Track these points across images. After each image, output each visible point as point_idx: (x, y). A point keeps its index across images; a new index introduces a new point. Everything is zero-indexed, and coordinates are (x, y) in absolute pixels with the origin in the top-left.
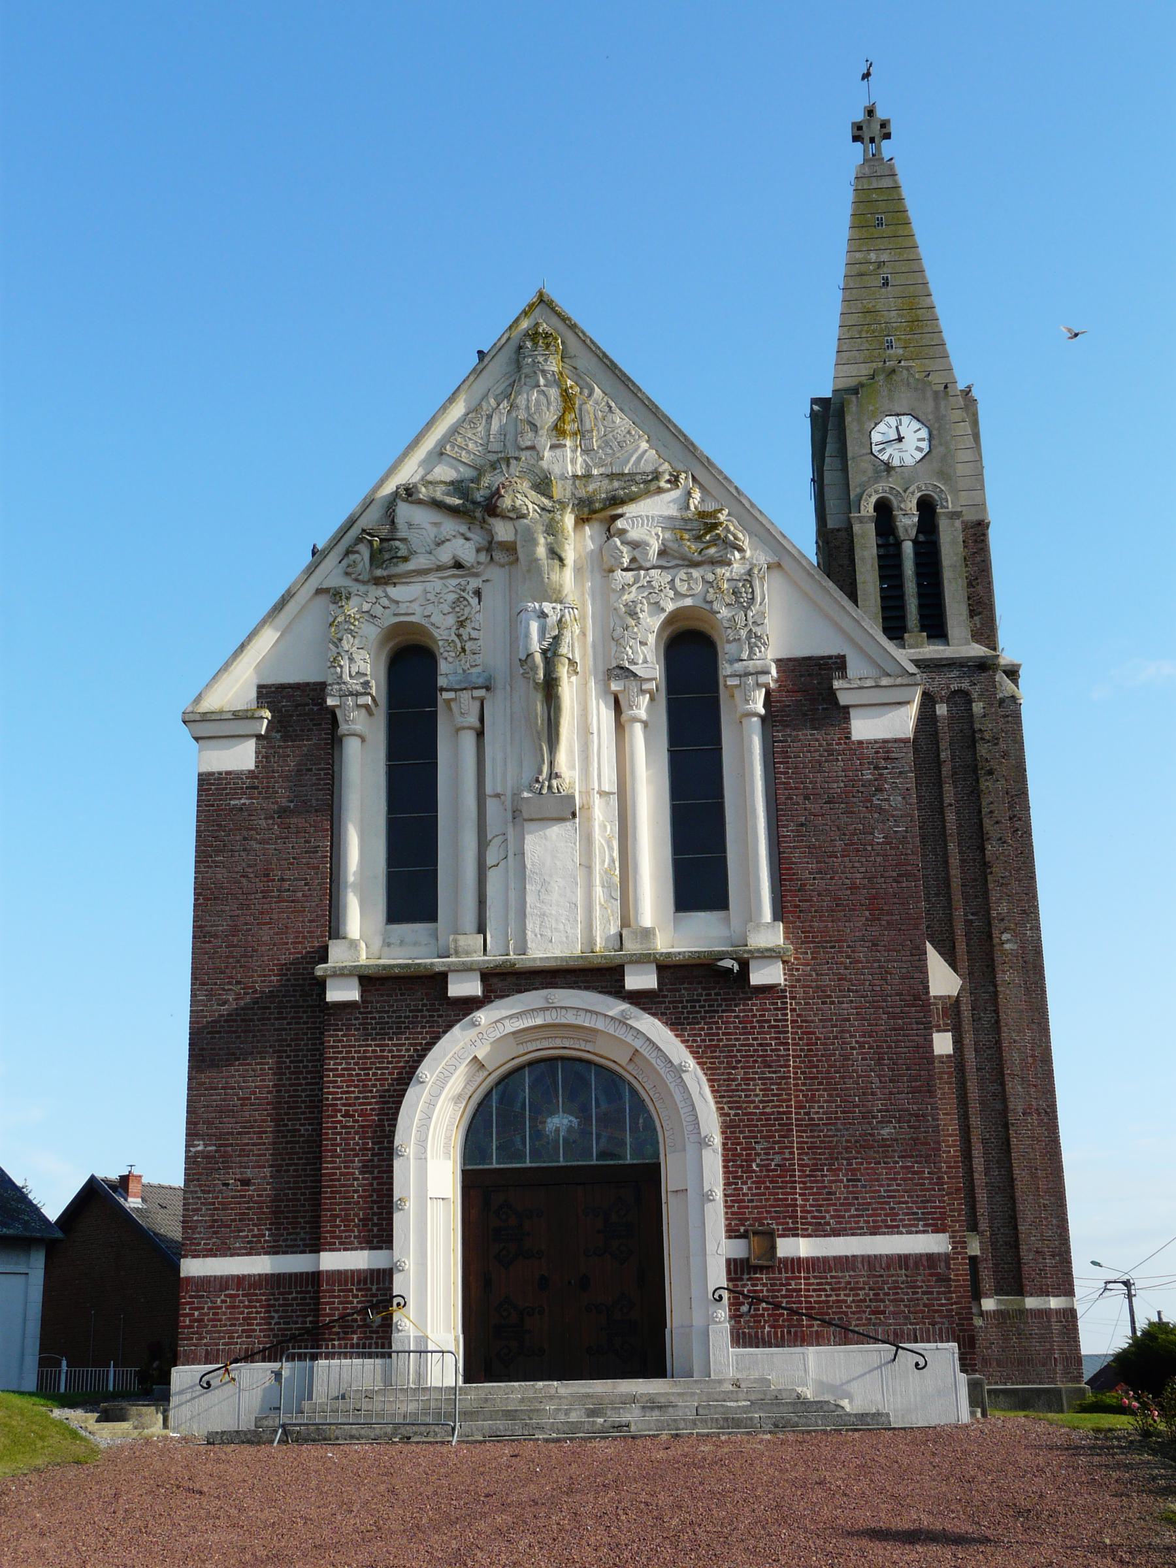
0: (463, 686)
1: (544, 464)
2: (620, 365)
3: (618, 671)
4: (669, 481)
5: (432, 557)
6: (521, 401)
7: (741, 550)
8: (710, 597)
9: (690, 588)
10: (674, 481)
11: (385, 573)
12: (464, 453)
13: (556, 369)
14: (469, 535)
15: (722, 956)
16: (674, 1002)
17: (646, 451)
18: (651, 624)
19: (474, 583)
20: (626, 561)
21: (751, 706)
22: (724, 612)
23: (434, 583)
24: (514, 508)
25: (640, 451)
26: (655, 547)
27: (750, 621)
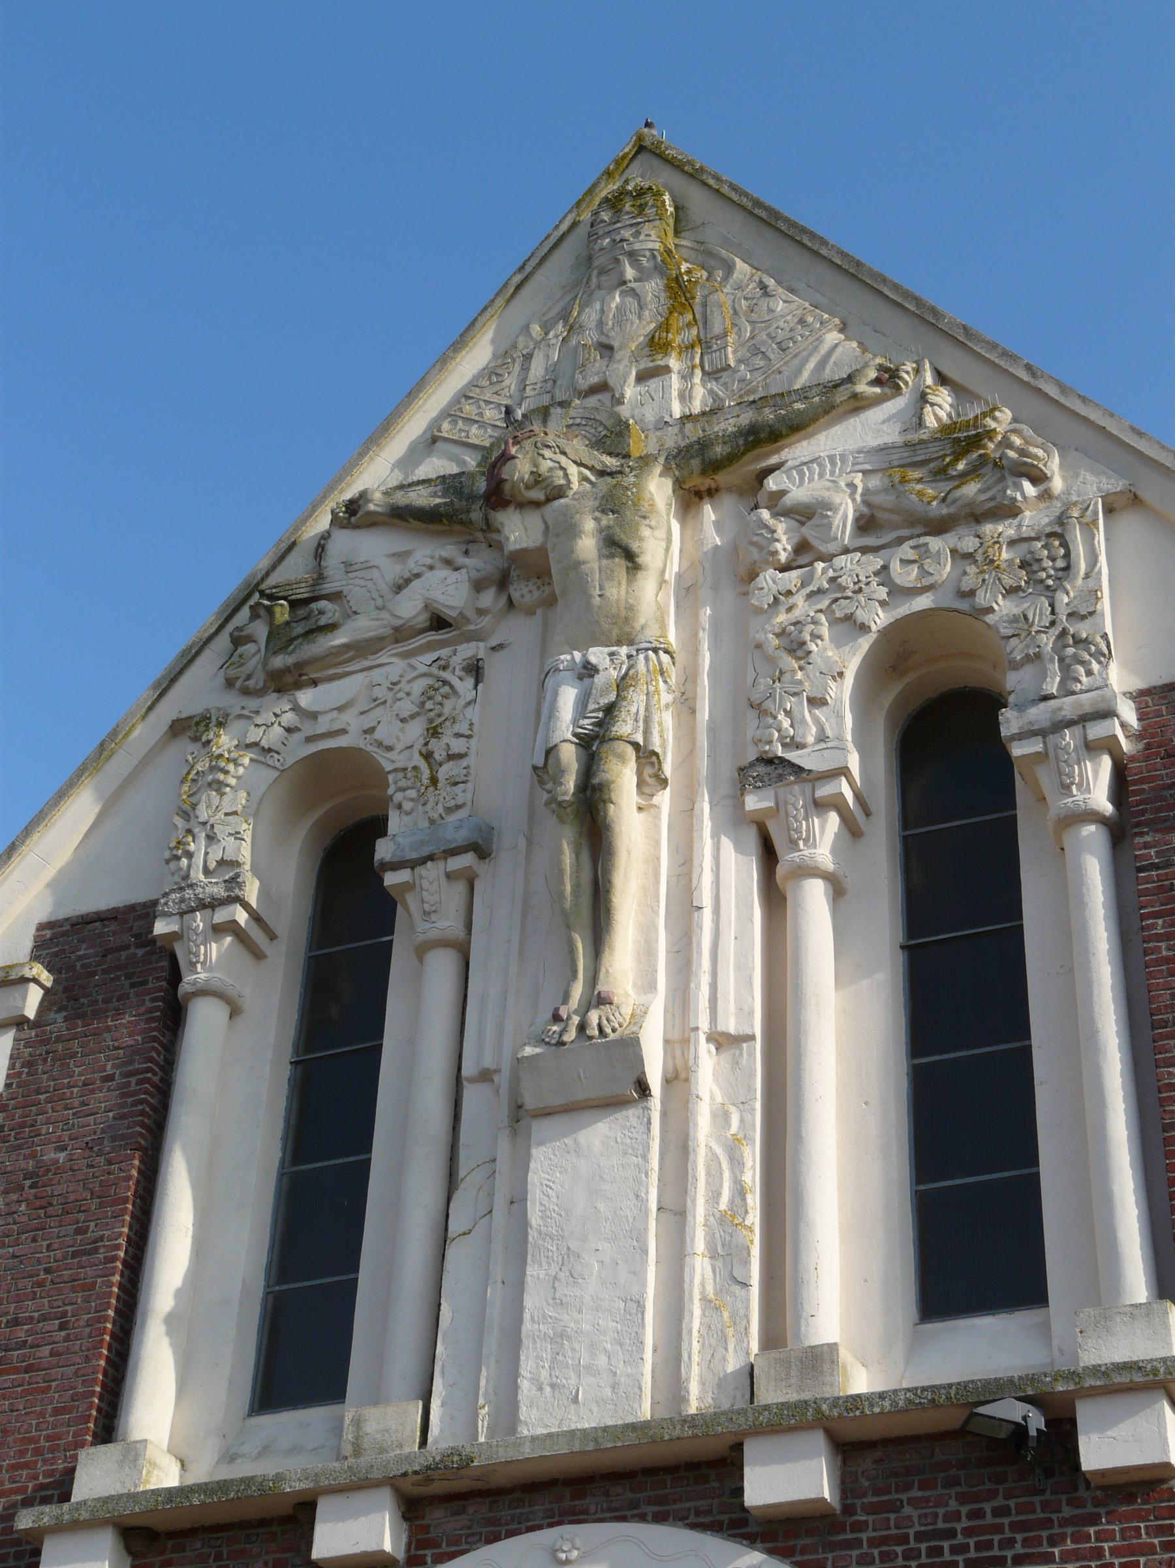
0: (426, 851)
1: (624, 411)
2: (787, 212)
3: (762, 769)
4: (877, 382)
5: (384, 615)
6: (590, 316)
7: (1038, 478)
8: (967, 584)
10: (889, 379)
12: (474, 429)
13: (657, 246)
14: (461, 560)
15: (995, 1389)
16: (883, 1541)
17: (836, 345)
19: (466, 651)
20: (784, 548)
22: (1004, 607)
23: (392, 665)
24: (538, 479)
25: (823, 350)
26: (846, 511)
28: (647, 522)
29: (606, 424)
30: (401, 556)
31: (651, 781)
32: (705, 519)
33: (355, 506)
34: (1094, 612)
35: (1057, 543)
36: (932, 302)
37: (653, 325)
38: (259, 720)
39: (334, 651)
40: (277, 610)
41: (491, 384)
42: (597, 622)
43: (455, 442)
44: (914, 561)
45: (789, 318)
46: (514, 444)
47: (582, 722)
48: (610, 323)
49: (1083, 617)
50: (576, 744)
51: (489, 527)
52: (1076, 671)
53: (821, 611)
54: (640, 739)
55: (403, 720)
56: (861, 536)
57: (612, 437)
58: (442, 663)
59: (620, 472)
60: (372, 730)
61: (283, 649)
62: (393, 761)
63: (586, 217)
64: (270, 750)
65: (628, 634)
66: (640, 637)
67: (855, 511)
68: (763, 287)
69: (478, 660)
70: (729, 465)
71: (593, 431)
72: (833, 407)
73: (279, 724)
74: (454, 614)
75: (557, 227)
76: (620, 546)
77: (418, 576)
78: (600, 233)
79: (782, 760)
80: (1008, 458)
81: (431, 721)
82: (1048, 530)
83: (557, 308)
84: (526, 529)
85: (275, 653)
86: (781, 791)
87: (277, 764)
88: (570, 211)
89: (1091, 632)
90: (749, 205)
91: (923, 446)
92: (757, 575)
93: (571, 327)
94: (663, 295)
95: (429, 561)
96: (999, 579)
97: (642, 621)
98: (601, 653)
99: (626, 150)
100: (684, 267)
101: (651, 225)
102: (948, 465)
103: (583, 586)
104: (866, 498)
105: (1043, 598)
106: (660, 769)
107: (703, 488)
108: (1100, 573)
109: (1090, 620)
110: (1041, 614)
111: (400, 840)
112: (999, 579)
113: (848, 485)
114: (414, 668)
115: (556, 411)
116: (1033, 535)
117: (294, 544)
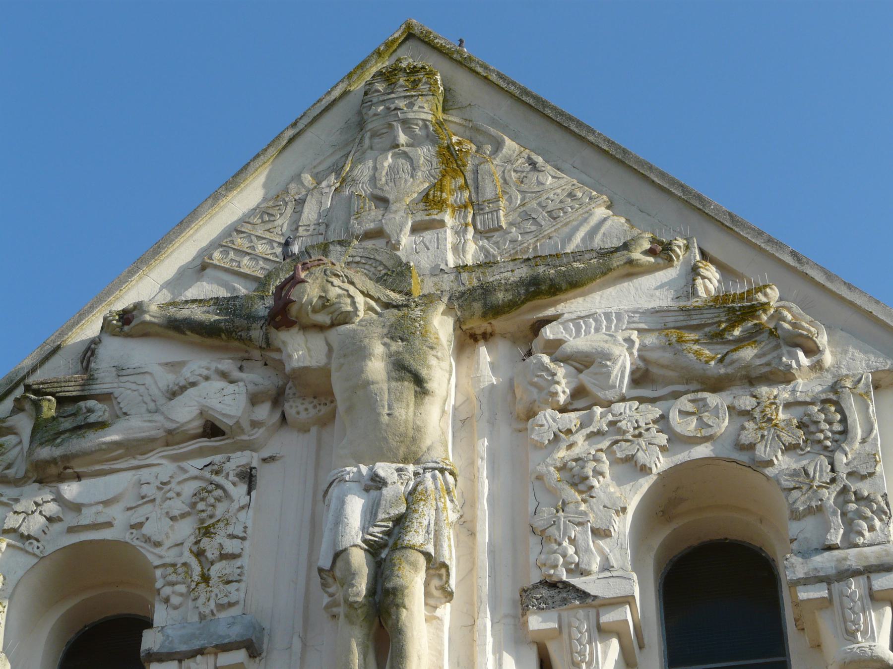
0: (196, 644)
2: (553, 102)
3: (545, 592)
4: (651, 252)
5: (158, 417)
7: (812, 351)
9: (702, 424)
11: (57, 452)
12: (246, 260)
14: (236, 374)
17: (605, 219)
18: (622, 501)
19: (240, 459)
20: (563, 391)
21: (863, 642)
24: (325, 303)
25: (593, 221)
26: (623, 363)
27: (843, 472)
28: (434, 352)
29: (387, 264)
30: (173, 366)
31: (436, 593)
32: (481, 359)
33: (130, 316)
34: (874, 473)
35: (833, 409)
36: (697, 190)
37: (426, 185)
38: (18, 507)
39: (104, 447)
40: (45, 404)
41: (263, 222)
42: (385, 439)
43: (226, 270)
44: (693, 414)
45: (559, 191)
46: (303, 269)
47: (371, 530)
48: (384, 179)
49: (863, 478)
50: (365, 550)
51: (268, 345)
52: (859, 525)
53: (601, 450)
54: (431, 549)
55: (173, 519)
56: (635, 388)
57: (396, 274)
58: (215, 467)
59: (407, 306)
60: (139, 526)
61: (51, 441)
62: (161, 557)
63: (358, 86)
64: (29, 537)
65: (415, 453)
66: (424, 459)
67: (632, 364)
68: (533, 164)
69: (251, 469)
70: (508, 312)
71: (373, 269)
72: (610, 270)
73: (41, 513)
74: (231, 422)
75: (329, 93)
76: (410, 372)
77: (193, 384)
78: (375, 100)
79: (566, 585)
80: (783, 328)
81: (202, 521)
82: (823, 396)
83: (329, 162)
84: (309, 350)
85: (41, 444)
86: (565, 614)
87: (37, 552)
88: (342, 81)
89: (872, 491)
90: (517, 93)
91: (697, 312)
92: (535, 414)
93: (344, 180)
94: (435, 161)
95: (205, 372)
96: (778, 436)
97: (428, 442)
98: (390, 468)
99: (396, 35)
100: (454, 139)
101: (424, 99)
102: (724, 330)
103: (371, 404)
104: (644, 353)
105: (822, 457)
106: (447, 582)
107: (478, 332)
108: (875, 439)
109: (868, 481)
110: (821, 471)
111: (169, 632)
112: (778, 436)
113: (625, 340)
114: (184, 471)
115: (336, 249)
116: (808, 399)
117: (59, 347)
